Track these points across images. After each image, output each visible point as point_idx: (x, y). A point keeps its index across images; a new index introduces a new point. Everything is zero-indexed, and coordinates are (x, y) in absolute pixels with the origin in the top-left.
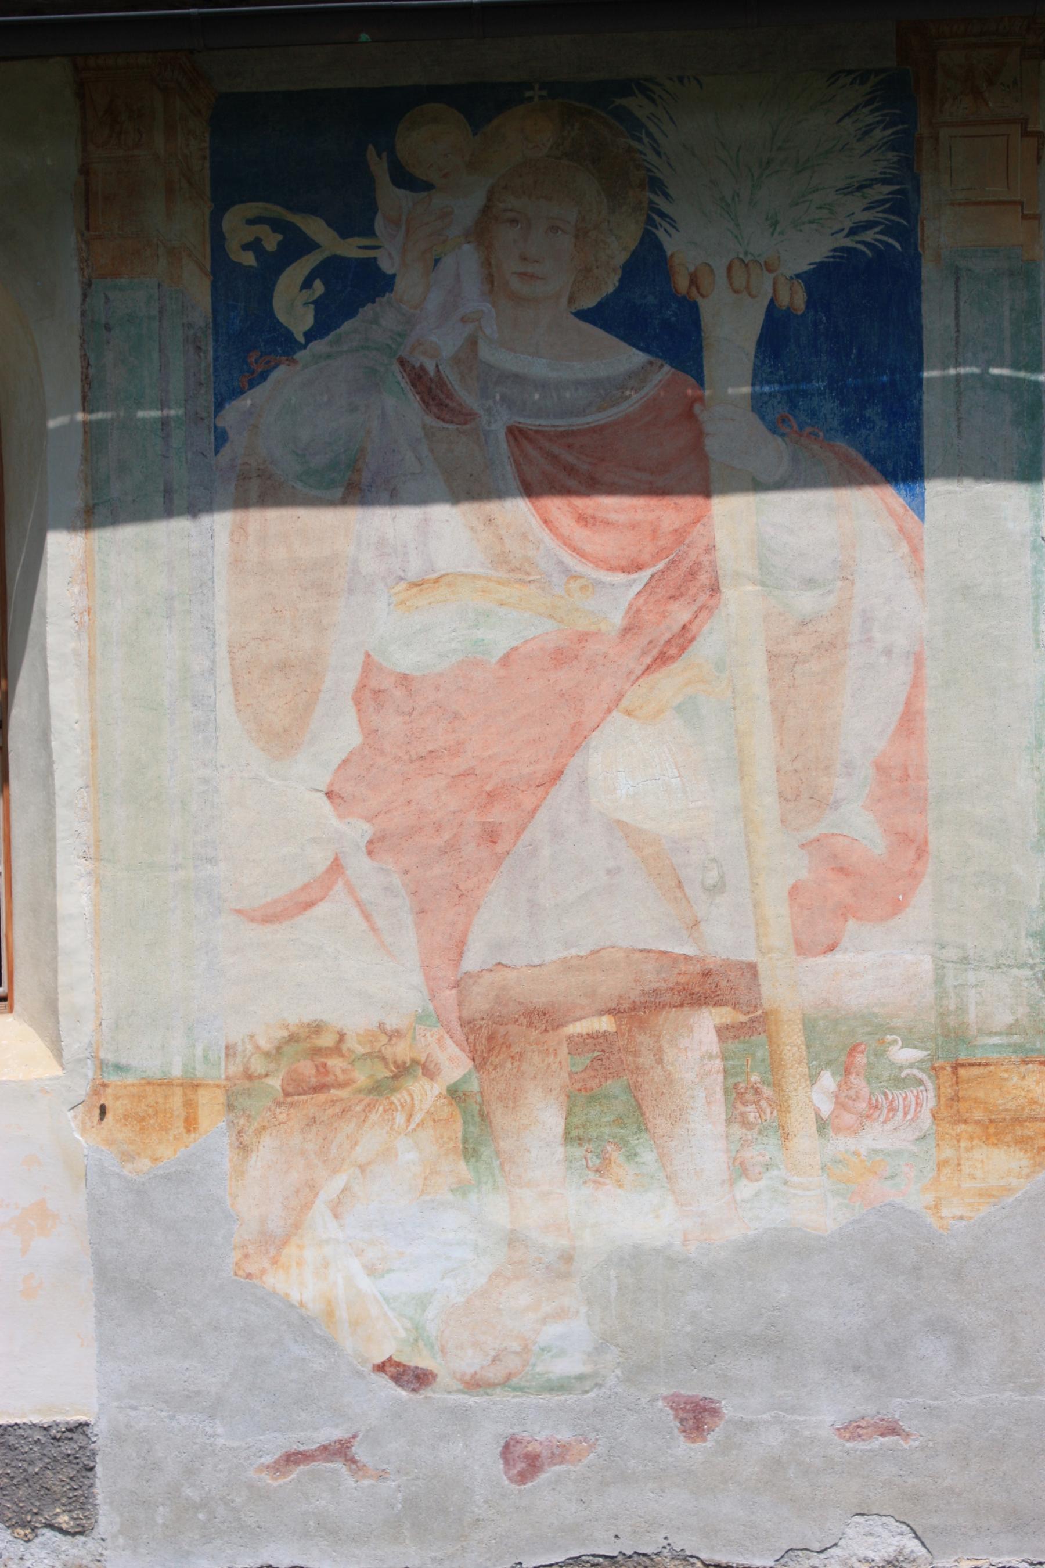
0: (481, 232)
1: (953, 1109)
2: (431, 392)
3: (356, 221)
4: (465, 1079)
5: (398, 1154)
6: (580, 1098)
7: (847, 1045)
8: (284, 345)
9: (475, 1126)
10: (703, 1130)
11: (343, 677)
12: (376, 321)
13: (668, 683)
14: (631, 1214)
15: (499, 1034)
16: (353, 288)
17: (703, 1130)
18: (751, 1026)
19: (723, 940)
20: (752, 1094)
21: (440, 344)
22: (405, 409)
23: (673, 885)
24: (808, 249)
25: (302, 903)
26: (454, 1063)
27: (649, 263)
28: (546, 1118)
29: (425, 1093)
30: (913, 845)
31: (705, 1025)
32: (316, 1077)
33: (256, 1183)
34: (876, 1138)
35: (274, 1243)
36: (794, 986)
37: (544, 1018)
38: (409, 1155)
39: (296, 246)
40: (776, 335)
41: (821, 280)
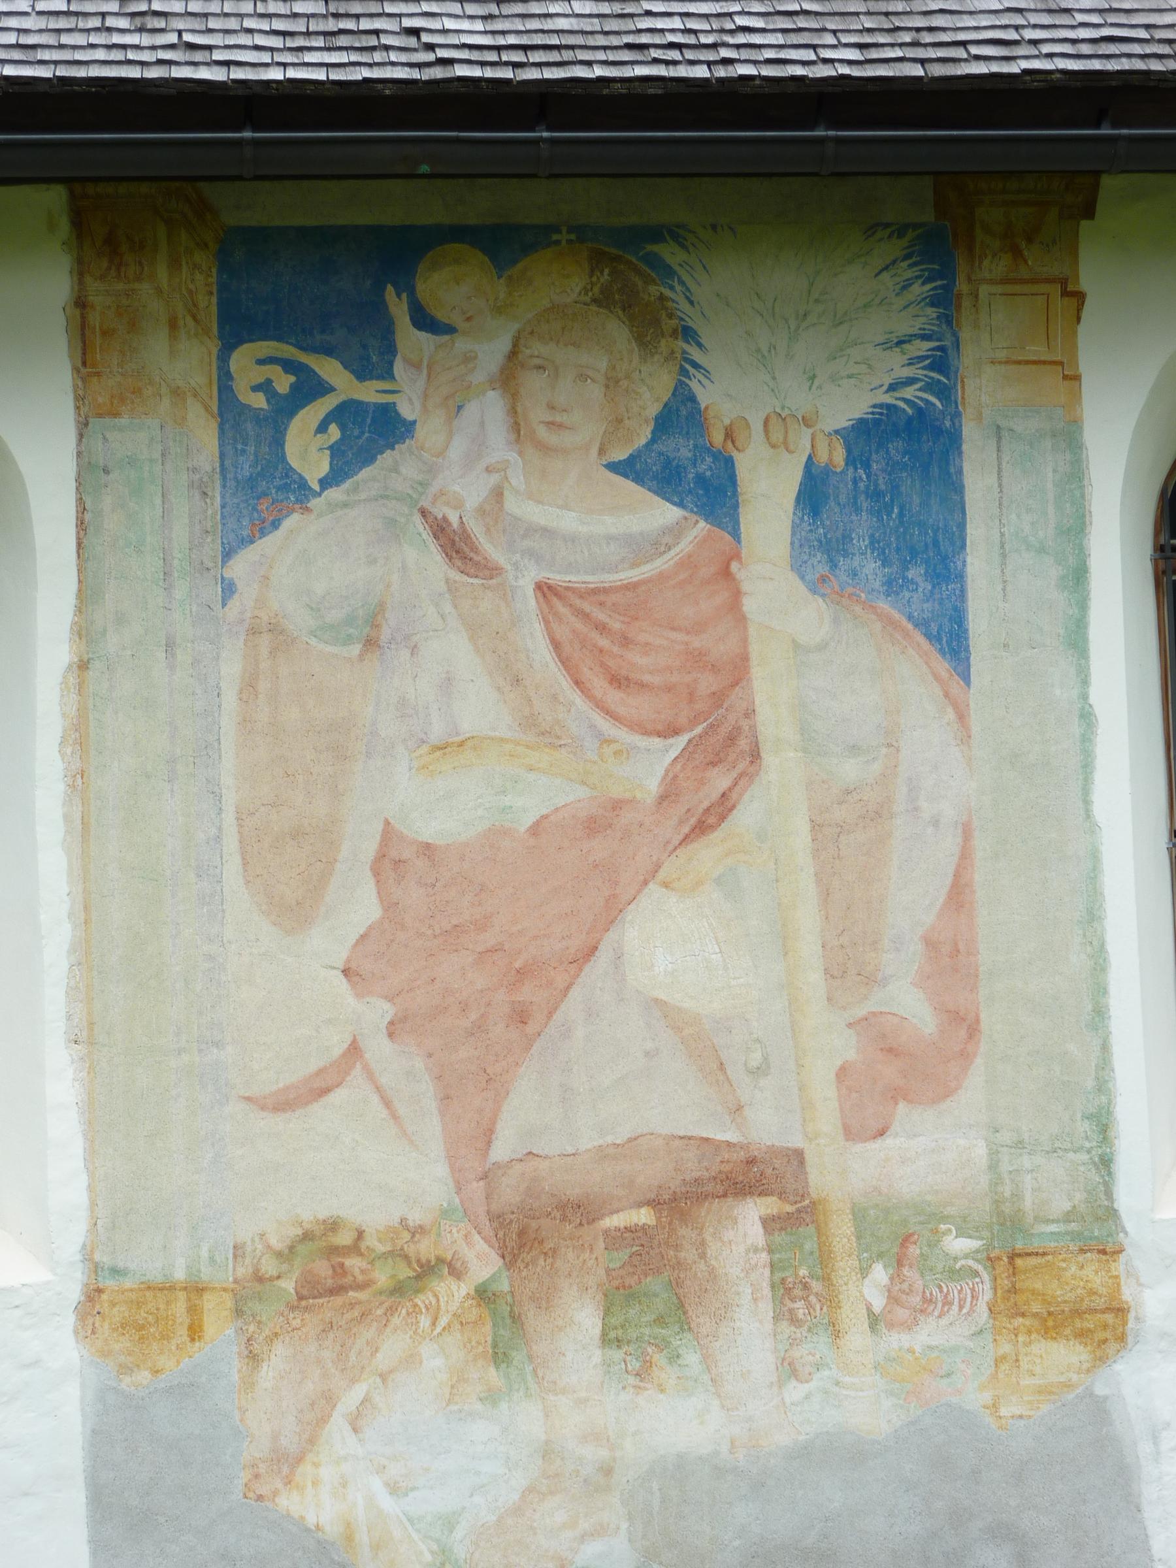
0: (508, 378)
1: (1010, 1304)
2: (455, 545)
3: (374, 360)
4: (493, 1278)
5: (420, 1363)
6: (618, 1297)
7: (900, 1237)
8: (298, 491)
9: (505, 1328)
10: (750, 1330)
11: (360, 844)
12: (396, 468)
13: (707, 854)
14: (676, 1420)
15: (531, 1229)
16: (372, 432)
17: (750, 1330)
18: (799, 1218)
19: (767, 1125)
20: (802, 1293)
21: (463, 493)
22: (427, 563)
23: (716, 1070)
24: (848, 404)
25: (317, 1088)
26: (482, 1262)
27: (680, 415)
28: (585, 1318)
29: (453, 1294)
30: (963, 1025)
31: (748, 1219)
32: (333, 1278)
33: (261, 1389)
34: (929, 1334)
35: (287, 1463)
36: (843, 1173)
37: (580, 1211)
38: (435, 1361)
39: (309, 388)
40: (813, 493)
41: (867, 435)
